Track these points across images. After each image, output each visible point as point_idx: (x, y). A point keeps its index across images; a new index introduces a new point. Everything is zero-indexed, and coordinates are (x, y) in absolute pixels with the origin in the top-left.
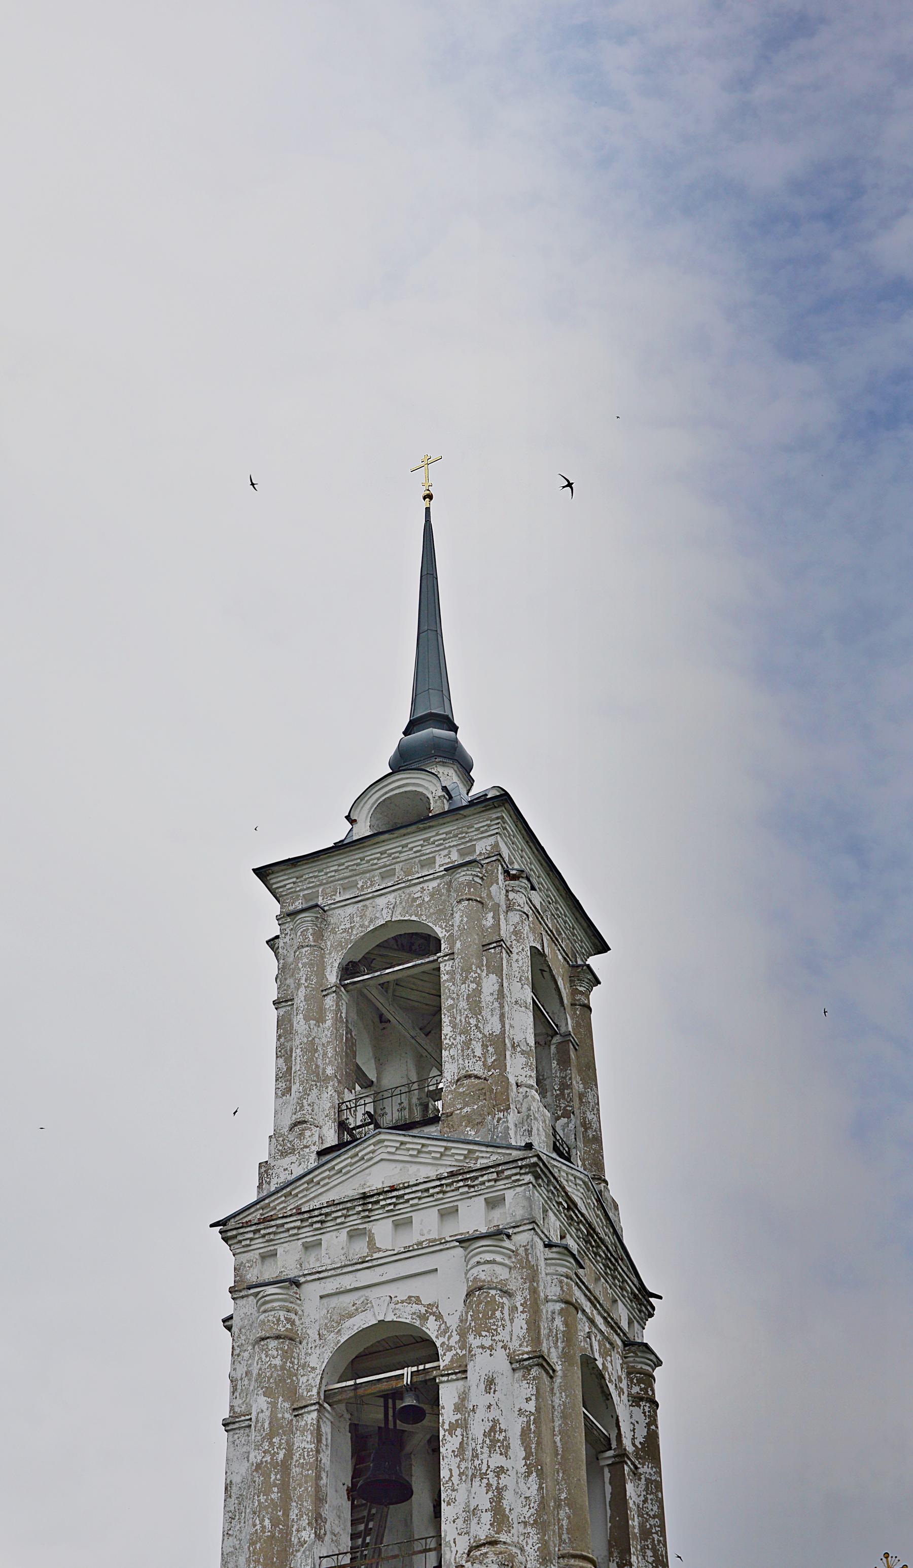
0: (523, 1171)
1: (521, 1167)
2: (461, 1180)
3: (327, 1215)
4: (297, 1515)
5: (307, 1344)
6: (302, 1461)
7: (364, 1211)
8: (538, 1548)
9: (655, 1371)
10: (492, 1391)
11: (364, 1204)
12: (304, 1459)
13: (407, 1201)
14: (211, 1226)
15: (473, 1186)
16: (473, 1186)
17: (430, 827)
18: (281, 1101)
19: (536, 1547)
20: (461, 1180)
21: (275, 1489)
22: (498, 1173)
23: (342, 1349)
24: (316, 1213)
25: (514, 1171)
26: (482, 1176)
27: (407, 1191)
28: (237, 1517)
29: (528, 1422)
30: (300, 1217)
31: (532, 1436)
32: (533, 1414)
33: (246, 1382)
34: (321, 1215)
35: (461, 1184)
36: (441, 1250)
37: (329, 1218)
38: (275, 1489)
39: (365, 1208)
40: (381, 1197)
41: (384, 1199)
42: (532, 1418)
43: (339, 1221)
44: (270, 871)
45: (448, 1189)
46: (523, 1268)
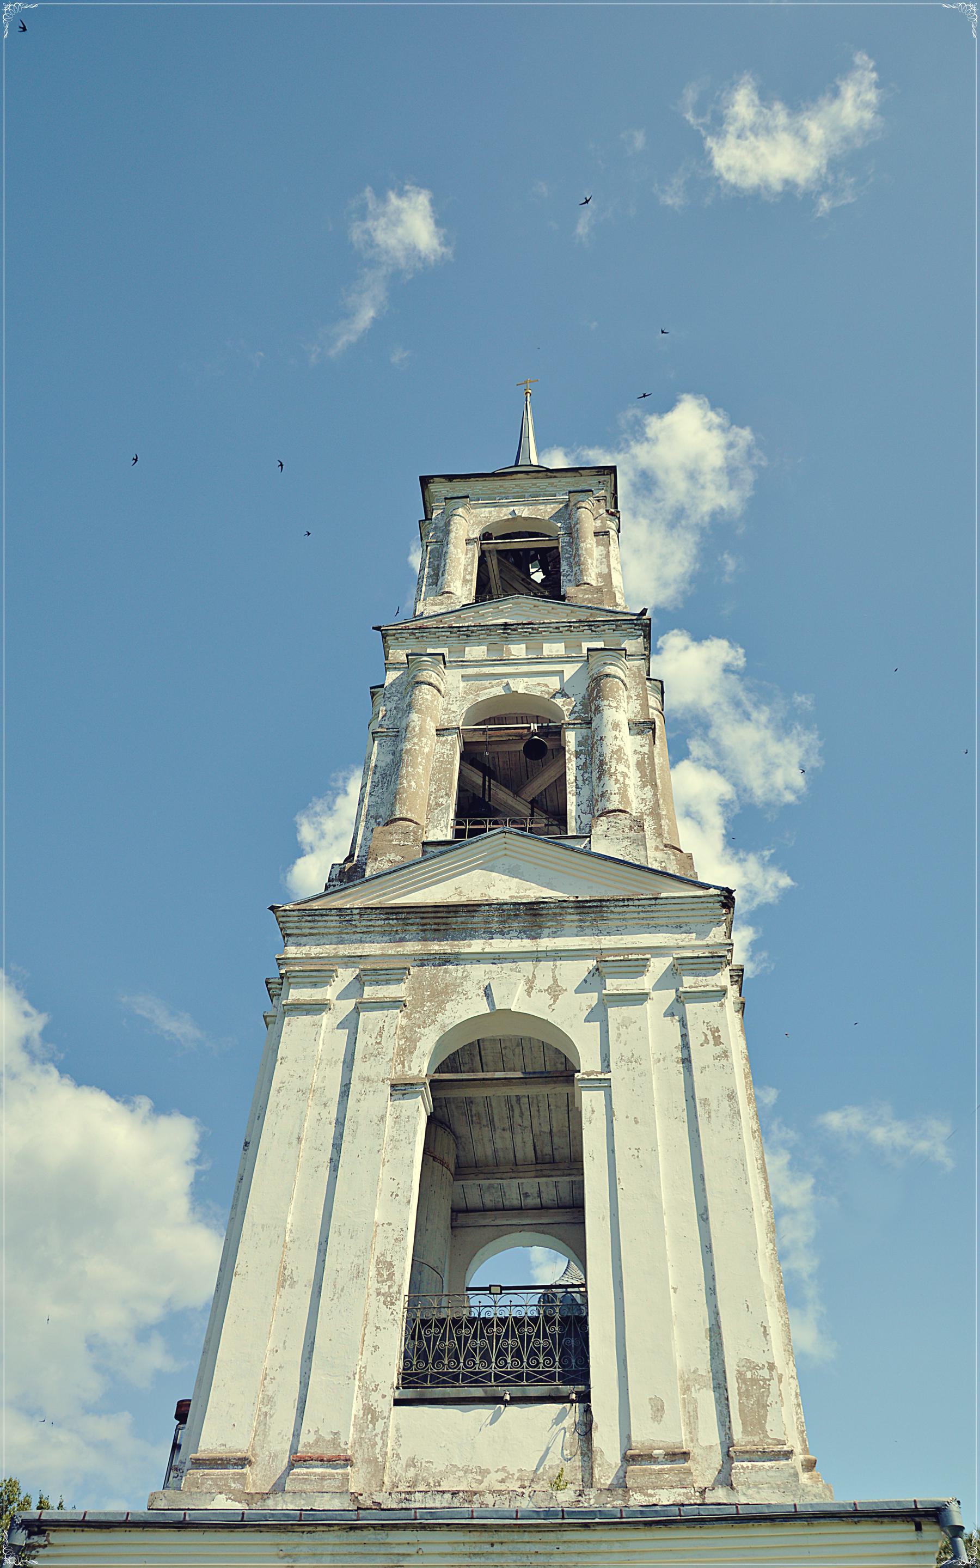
0: (637, 627)
1: (636, 625)
2: (587, 625)
3: (472, 632)
4: (435, 789)
5: (449, 698)
6: (441, 759)
7: (504, 633)
8: (654, 829)
9: (456, 1050)
10: (618, 730)
11: (504, 629)
12: (444, 758)
13: (541, 632)
14: (374, 628)
15: (595, 631)
16: (595, 631)
17: (555, 477)
18: (428, 588)
19: (652, 828)
20: (587, 625)
21: (421, 767)
22: (616, 626)
23: (477, 707)
24: (464, 629)
25: (630, 626)
26: (604, 625)
27: (541, 626)
28: (380, 785)
29: (643, 758)
30: (450, 629)
31: (647, 765)
32: (646, 754)
33: (395, 712)
34: (468, 630)
35: (587, 628)
36: (567, 661)
37: (474, 634)
38: (421, 767)
39: (505, 631)
40: (520, 627)
41: (522, 628)
42: (646, 756)
43: (481, 636)
44: (432, 481)
45: (575, 629)
46: (636, 677)
